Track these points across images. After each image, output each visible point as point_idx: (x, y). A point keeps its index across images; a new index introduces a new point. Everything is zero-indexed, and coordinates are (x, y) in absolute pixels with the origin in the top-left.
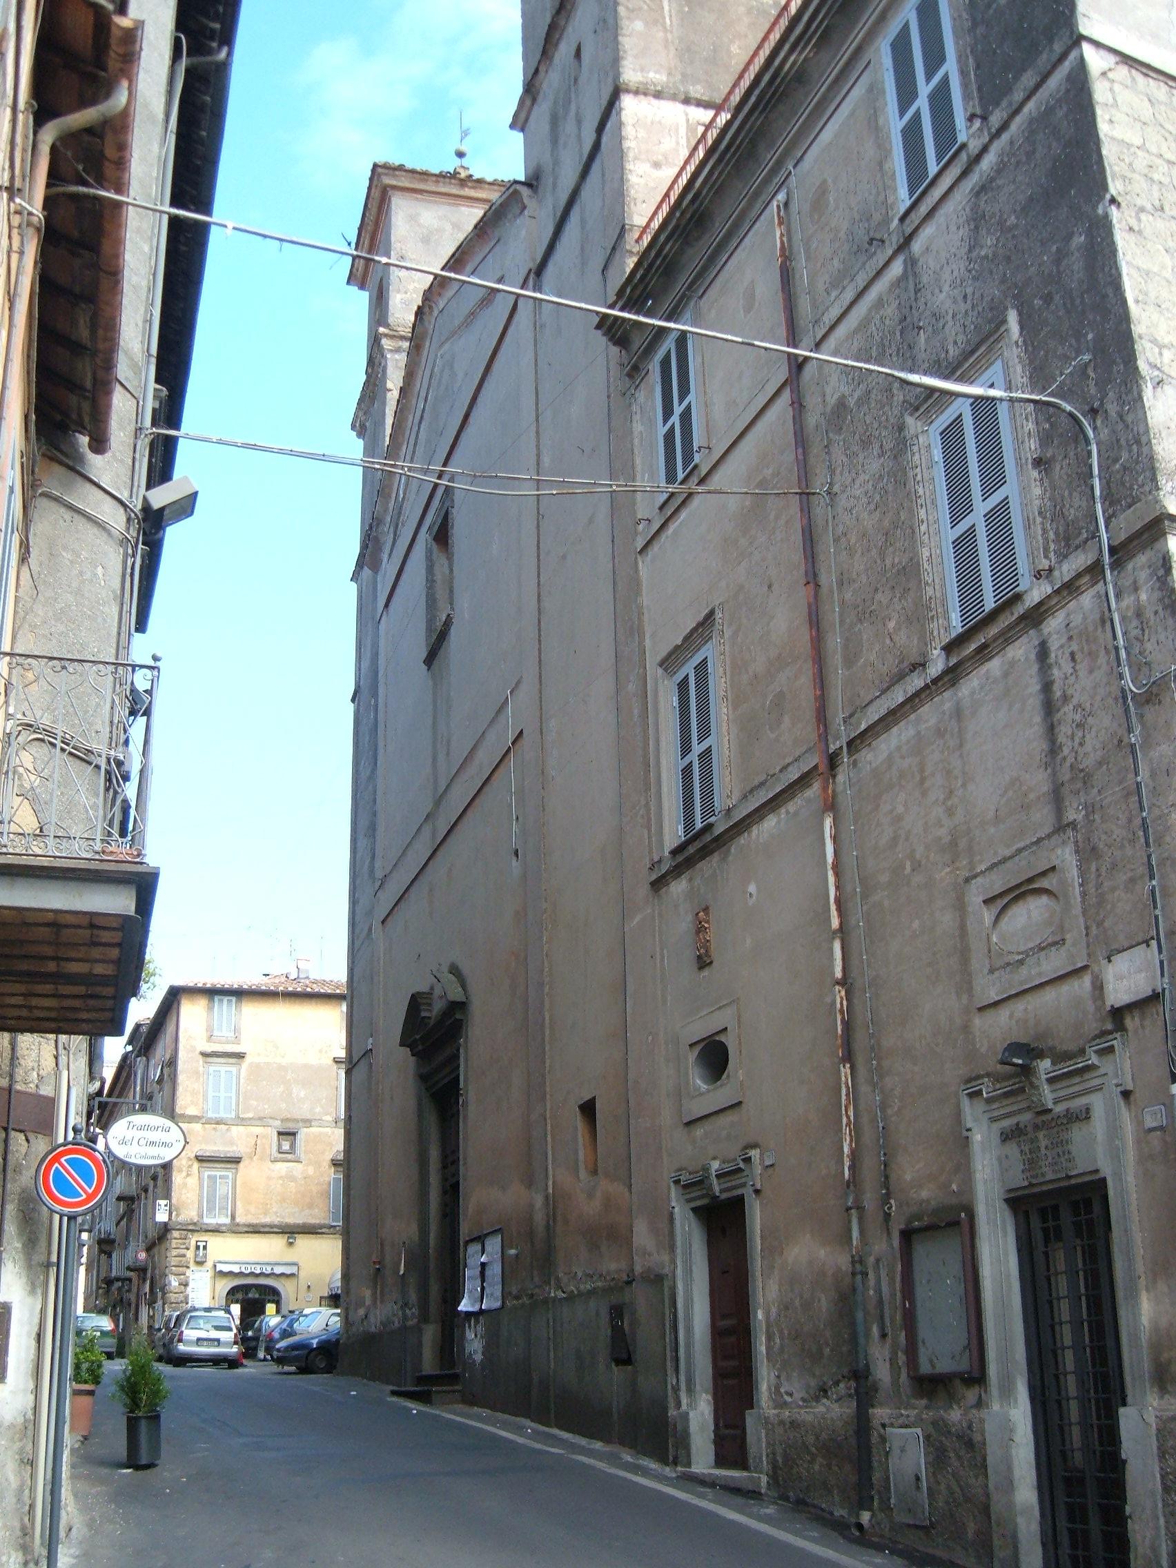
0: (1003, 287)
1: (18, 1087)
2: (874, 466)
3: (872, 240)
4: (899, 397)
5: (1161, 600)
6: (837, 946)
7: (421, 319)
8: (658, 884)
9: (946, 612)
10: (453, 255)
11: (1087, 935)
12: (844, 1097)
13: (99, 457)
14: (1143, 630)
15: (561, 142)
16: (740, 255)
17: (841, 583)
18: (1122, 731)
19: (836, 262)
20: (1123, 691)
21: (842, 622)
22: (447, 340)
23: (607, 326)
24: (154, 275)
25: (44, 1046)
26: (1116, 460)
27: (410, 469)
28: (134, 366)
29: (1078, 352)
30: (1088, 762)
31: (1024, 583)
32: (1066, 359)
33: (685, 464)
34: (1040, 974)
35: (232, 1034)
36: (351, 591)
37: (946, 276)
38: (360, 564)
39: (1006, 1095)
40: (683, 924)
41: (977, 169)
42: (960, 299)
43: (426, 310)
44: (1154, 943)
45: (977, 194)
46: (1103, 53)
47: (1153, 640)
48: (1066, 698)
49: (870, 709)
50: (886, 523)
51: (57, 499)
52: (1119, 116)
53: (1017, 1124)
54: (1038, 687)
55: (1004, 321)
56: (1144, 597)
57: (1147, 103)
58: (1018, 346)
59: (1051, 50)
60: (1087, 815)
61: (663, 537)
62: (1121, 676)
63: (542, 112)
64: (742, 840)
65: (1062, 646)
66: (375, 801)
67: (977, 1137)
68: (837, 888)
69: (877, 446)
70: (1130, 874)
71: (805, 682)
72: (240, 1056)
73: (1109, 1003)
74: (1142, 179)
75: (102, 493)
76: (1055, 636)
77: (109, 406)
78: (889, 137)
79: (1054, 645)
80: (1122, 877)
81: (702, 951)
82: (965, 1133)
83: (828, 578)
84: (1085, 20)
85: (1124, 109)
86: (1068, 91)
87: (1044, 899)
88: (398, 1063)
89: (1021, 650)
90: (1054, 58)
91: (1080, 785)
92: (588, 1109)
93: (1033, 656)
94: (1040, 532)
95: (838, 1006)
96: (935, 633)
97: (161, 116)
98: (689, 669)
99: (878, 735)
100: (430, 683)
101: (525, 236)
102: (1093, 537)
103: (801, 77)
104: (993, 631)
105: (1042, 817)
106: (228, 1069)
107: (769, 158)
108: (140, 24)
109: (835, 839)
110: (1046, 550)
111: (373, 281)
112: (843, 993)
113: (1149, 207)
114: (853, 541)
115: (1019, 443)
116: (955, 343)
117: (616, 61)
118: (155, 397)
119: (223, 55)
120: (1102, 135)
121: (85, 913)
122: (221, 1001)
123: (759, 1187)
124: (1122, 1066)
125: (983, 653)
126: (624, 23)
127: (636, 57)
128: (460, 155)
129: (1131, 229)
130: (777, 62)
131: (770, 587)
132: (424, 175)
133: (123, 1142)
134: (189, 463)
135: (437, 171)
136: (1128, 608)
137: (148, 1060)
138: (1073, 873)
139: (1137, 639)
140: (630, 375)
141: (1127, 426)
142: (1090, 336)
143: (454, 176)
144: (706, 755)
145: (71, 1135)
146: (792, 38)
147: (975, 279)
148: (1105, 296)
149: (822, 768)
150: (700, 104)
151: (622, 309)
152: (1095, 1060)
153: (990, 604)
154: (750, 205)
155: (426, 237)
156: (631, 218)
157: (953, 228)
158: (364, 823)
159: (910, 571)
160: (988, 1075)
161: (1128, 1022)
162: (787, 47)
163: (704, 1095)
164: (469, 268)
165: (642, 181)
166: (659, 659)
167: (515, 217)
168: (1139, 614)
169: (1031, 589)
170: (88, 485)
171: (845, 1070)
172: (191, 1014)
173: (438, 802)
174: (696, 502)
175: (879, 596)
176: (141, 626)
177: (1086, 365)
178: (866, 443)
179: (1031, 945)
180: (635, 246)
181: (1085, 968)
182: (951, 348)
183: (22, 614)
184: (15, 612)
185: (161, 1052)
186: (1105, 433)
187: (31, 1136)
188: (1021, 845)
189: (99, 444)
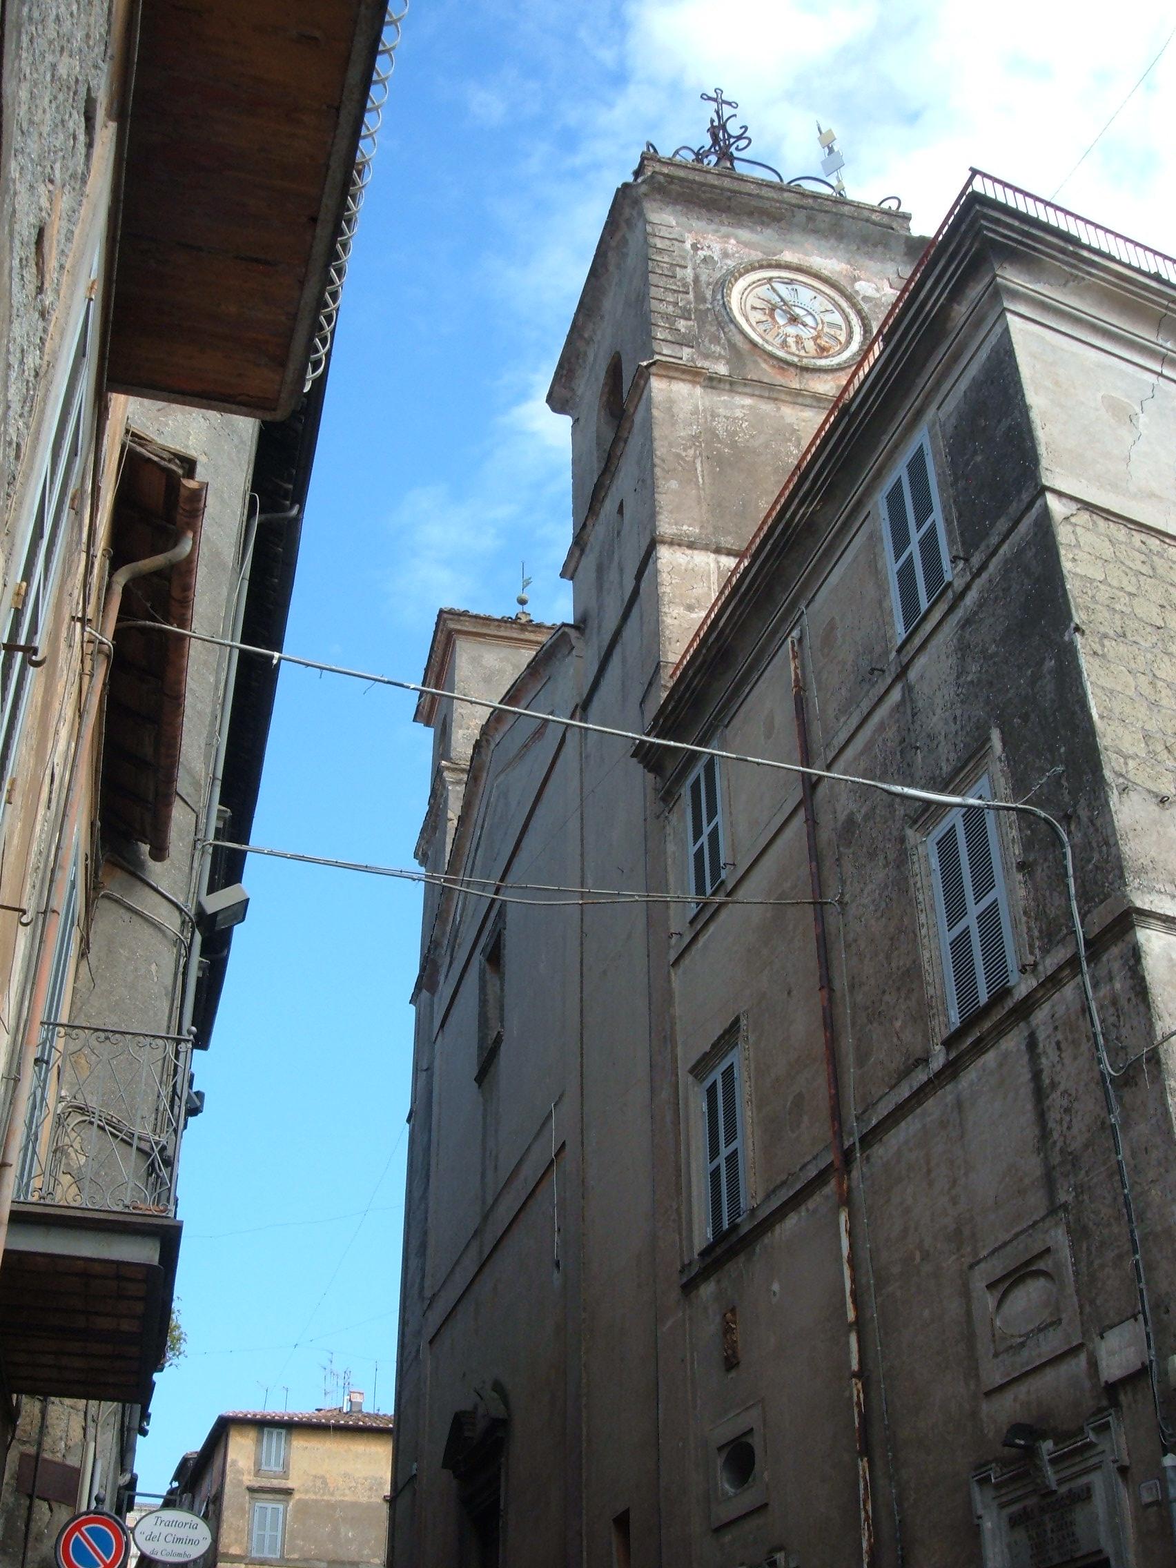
0: (988, 709)
1: (47, 1455)
3: (873, 670)
4: (900, 811)
5: (1133, 988)
6: (853, 1339)
7: (479, 753)
8: (689, 1287)
10: (508, 693)
11: (1081, 1313)
12: (862, 1492)
13: (159, 864)
14: (1118, 1016)
15: (606, 586)
17: (852, 987)
18: (1103, 1114)
19: (843, 691)
20: (1102, 1074)
21: (853, 1024)
22: (502, 771)
23: (644, 754)
25: (74, 1417)
26: (1089, 861)
28: (196, 785)
29: (1053, 764)
30: (1075, 1145)
32: (1042, 771)
34: (1039, 1355)
35: (280, 1469)
36: (409, 1014)
37: (939, 701)
38: (419, 987)
39: (1013, 1479)
40: (710, 1327)
41: (962, 604)
43: (484, 743)
44: (1141, 1317)
45: (963, 627)
46: (1064, 500)
47: (1128, 1026)
48: (1054, 1085)
49: (880, 1105)
51: (117, 901)
52: (1080, 555)
53: (1025, 1508)
54: (1029, 1076)
55: (989, 739)
56: (1118, 986)
58: (1001, 761)
59: (1020, 500)
60: (1077, 1196)
61: (694, 949)
62: (1100, 1061)
63: (589, 562)
64: (767, 1240)
65: (1049, 1037)
66: (426, 1219)
67: (988, 1525)
68: (853, 1281)
69: (881, 857)
70: (1116, 1252)
71: (822, 1081)
72: (288, 1492)
73: (1103, 1380)
74: (1104, 610)
75: (159, 897)
76: (1042, 1027)
77: (169, 817)
78: (886, 578)
79: (1041, 1035)
80: (1111, 1254)
81: (730, 1352)
82: (976, 1521)
84: (1048, 473)
85: (1086, 549)
86: (1036, 534)
87: (1041, 1282)
88: (439, 1483)
89: (1013, 1042)
90: (1023, 506)
91: (1069, 1167)
92: (622, 1522)
93: (1023, 1047)
94: (1025, 930)
95: (855, 1398)
96: (937, 1030)
98: (717, 1075)
99: (888, 1131)
100: (481, 1099)
101: (573, 673)
103: (811, 527)
104: (987, 1025)
105: (1036, 1201)
106: (275, 1506)
107: (785, 599)
109: (850, 1233)
110: (1031, 946)
111: (437, 719)
112: (860, 1386)
113: (1111, 633)
114: (862, 947)
115: (1004, 848)
116: (948, 760)
117: (653, 516)
118: (219, 818)
119: (295, 511)
120: (1065, 572)
121: (113, 1262)
122: (270, 1434)
123: (1126, 1462)
124: (1118, 1442)
125: (980, 1047)
126: (660, 482)
127: (671, 512)
128: (522, 602)
129: (1095, 653)
131: (789, 993)
132: (487, 620)
133: (150, 1538)
136: (1105, 997)
137: (193, 1497)
138: (1066, 1253)
139: (1114, 1025)
140: (664, 799)
141: (1097, 830)
142: (1063, 750)
144: (732, 1158)
145: (94, 1504)
146: (801, 494)
147: (962, 702)
148: (1074, 713)
149: (837, 1164)
150: (729, 553)
151: (657, 736)
152: (1092, 1437)
155: (485, 675)
156: (666, 655)
157: (943, 657)
158: (415, 1243)
159: (912, 975)
160: (996, 1460)
161: (1123, 1398)
162: (797, 501)
163: (733, 1500)
164: (524, 703)
165: (676, 622)
166: (689, 1066)
167: (565, 657)
168: (1114, 1002)
169: (1019, 984)
170: (147, 889)
171: (863, 1464)
172: (241, 1452)
173: (485, 1218)
174: (723, 915)
175: (887, 998)
176: (202, 1041)
177: (1060, 776)
178: (872, 855)
179: (1031, 1327)
180: (667, 680)
181: (1081, 1346)
183: (79, 1004)
184: (73, 1003)
185: (207, 1487)
186: (1078, 838)
187: (55, 1505)
188: (1018, 1229)
189: (159, 853)
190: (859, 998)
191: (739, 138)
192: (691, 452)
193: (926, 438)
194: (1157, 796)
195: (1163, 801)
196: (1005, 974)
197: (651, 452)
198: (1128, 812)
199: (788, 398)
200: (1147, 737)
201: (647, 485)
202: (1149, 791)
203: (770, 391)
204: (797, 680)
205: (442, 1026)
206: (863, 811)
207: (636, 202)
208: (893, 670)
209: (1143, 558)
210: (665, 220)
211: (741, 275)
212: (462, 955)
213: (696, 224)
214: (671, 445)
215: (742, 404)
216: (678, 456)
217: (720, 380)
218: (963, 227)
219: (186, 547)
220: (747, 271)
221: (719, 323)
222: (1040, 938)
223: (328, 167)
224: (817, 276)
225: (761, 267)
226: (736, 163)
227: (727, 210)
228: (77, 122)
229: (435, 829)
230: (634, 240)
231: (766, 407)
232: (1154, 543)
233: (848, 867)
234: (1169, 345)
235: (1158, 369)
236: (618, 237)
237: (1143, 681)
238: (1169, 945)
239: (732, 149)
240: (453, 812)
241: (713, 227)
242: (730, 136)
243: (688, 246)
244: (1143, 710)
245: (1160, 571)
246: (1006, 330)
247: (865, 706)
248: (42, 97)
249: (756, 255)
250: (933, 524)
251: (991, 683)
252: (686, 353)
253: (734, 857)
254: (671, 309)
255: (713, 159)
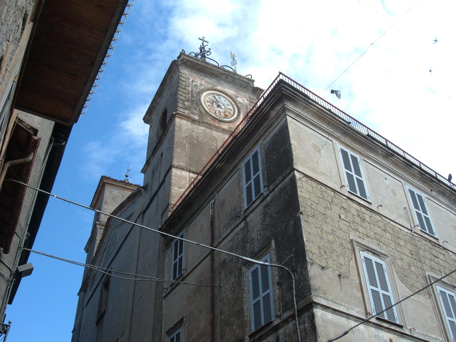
2: (233, 280)
3: (236, 216)
5: (311, 327)
9: (250, 325)
15: (155, 177)
16: (200, 216)
17: (221, 313)
19: (226, 221)
21: (220, 325)
24: (33, 202)
26: (300, 285)
27: (98, 269)
28: (22, 229)
29: (291, 254)
31: (273, 318)
33: (179, 275)
38: (81, 290)
41: (266, 200)
42: (259, 235)
45: (265, 207)
46: (300, 173)
47: (309, 338)
50: (235, 297)
52: (303, 190)
55: (271, 243)
56: (306, 325)
57: (311, 187)
63: (150, 169)
65: (283, 338)
69: (234, 274)
78: (243, 188)
79: (281, 337)
83: (217, 312)
85: (305, 188)
86: (290, 182)
90: (287, 174)
97: (42, 159)
102: (293, 307)
103: (221, 170)
104: (264, 332)
108: (40, 139)
113: (311, 215)
114: (225, 301)
115: (273, 277)
117: (172, 159)
118: (26, 236)
119: (64, 144)
126: (175, 149)
127: (177, 158)
128: (127, 176)
130: (214, 165)
131: (200, 312)
132: (116, 181)
134: (32, 259)
135: (119, 180)
136: (302, 328)
141: (303, 276)
142: (294, 249)
143: (124, 182)
146: (219, 160)
147: (263, 230)
150: (193, 172)
153: (263, 324)
154: (204, 202)
155: (113, 199)
156: (171, 201)
157: (258, 215)
159: (240, 313)
162: (217, 162)
168: (305, 330)
174: (181, 285)
175: (232, 318)
176: (10, 302)
178: (230, 273)
180: (172, 209)
182: (256, 248)
186: (297, 277)
190: (223, 317)
191: (208, 52)
192: (185, 141)
193: (259, 148)
194: (321, 266)
195: (323, 268)
196: (270, 317)
197: (173, 140)
198: (313, 271)
199: (215, 129)
200: (319, 248)
201: (171, 149)
202: (319, 265)
203: (210, 126)
204: (212, 215)
205: (87, 304)
206: (229, 259)
207: (177, 66)
208: (242, 217)
209: (321, 193)
210: (185, 72)
211: (205, 91)
212: (96, 283)
213: (193, 74)
214: (179, 138)
215: (201, 129)
216: (181, 142)
217: (196, 121)
218: (277, 89)
219: (31, 157)
220: (207, 90)
221: (197, 104)
222: (283, 307)
223: (100, 48)
224: (226, 94)
225: (211, 90)
226: (206, 59)
227: (203, 72)
228: (20, 22)
229: (92, 242)
230: (175, 76)
231: (208, 131)
232: (324, 188)
233: (223, 276)
234: (330, 130)
235: (327, 137)
236: (170, 75)
237: (319, 230)
238: (323, 313)
239: (206, 55)
240: (99, 238)
241: (198, 76)
242: (205, 51)
243: (191, 81)
244: (319, 239)
245: (325, 197)
246: (286, 121)
247: (233, 227)
248: (11, 12)
249: (210, 86)
250: (259, 175)
251: (273, 225)
252: (187, 112)
253: (187, 267)
254: (184, 98)
255: (200, 57)
